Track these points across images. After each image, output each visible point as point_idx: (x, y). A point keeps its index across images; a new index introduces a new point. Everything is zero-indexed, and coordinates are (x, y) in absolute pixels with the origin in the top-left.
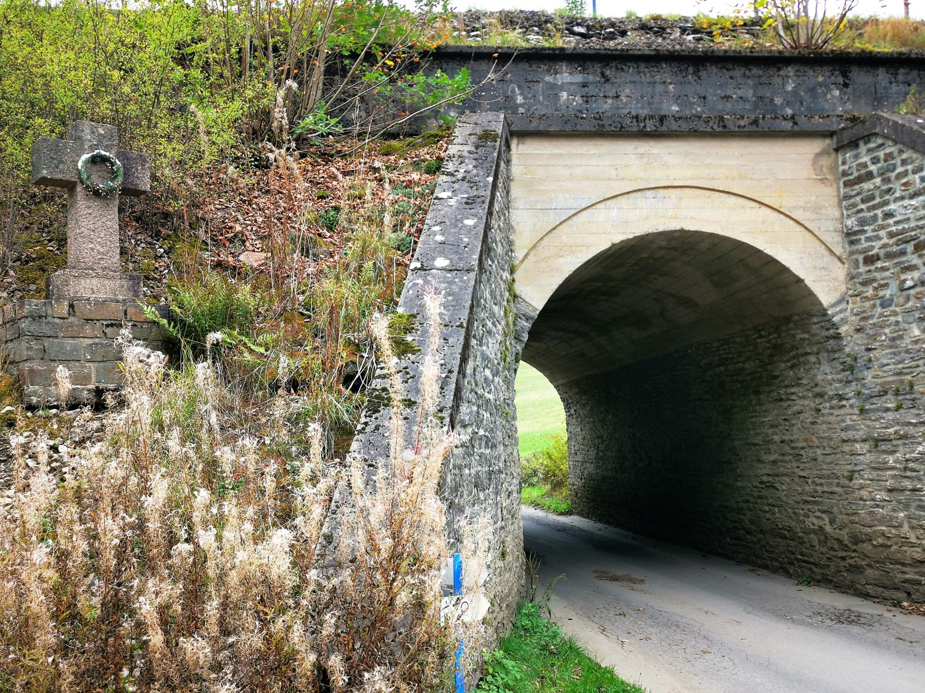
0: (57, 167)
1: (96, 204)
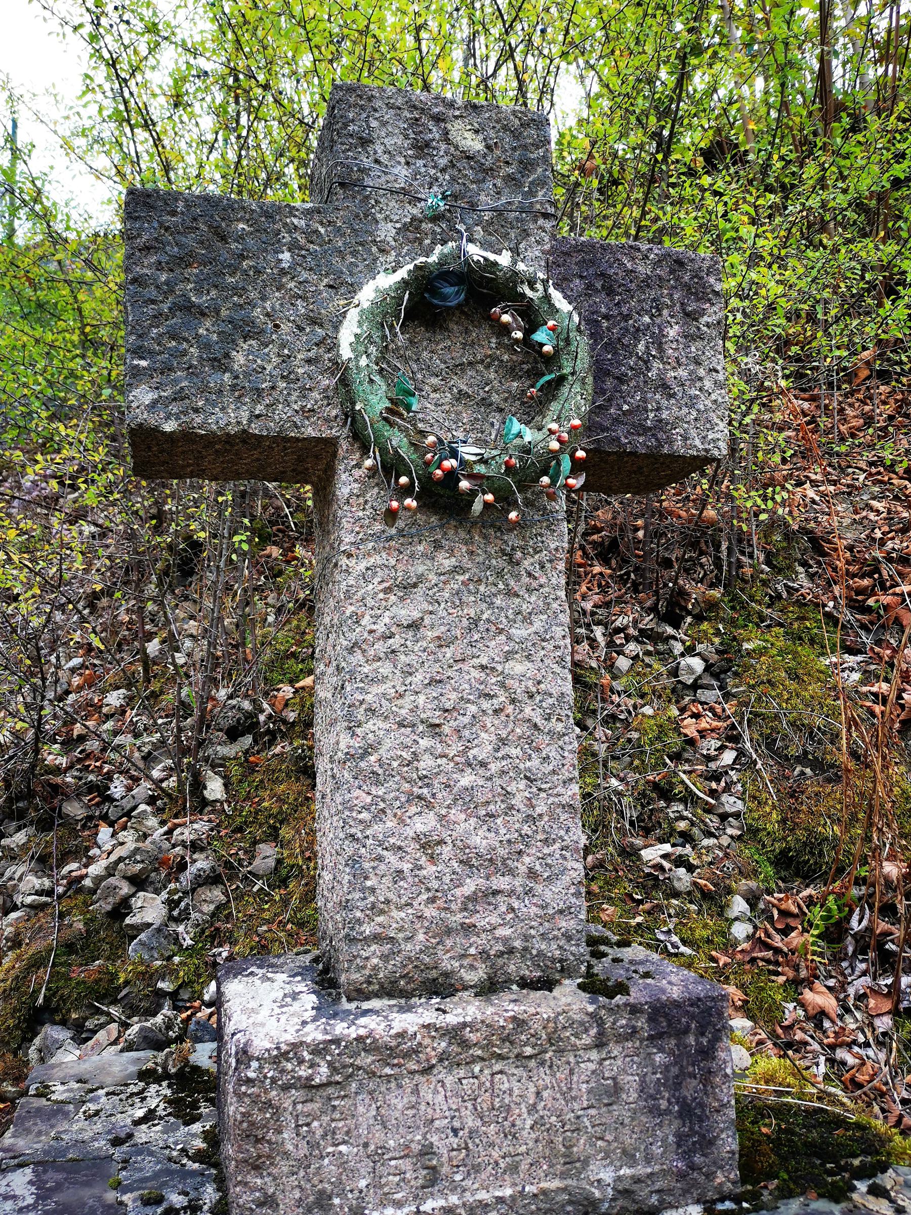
0: (221, 363)
1: (441, 562)
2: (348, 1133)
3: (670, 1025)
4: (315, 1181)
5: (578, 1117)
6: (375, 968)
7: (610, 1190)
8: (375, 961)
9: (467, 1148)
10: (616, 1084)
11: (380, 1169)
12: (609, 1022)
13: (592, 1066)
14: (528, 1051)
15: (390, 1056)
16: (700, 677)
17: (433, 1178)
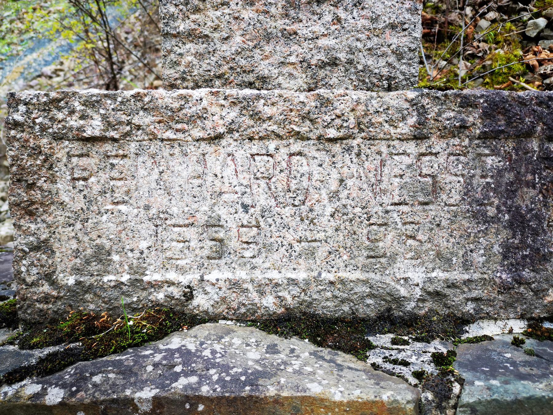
2: (128, 192)
3: (509, 123)
4: (94, 235)
5: (387, 212)
6: (189, 64)
7: (417, 289)
8: (190, 58)
9: (258, 227)
10: (435, 183)
11: (163, 235)
12: (433, 110)
13: (407, 160)
14: (332, 133)
15: (172, 118)
16: (542, 31)
17: (220, 250)
